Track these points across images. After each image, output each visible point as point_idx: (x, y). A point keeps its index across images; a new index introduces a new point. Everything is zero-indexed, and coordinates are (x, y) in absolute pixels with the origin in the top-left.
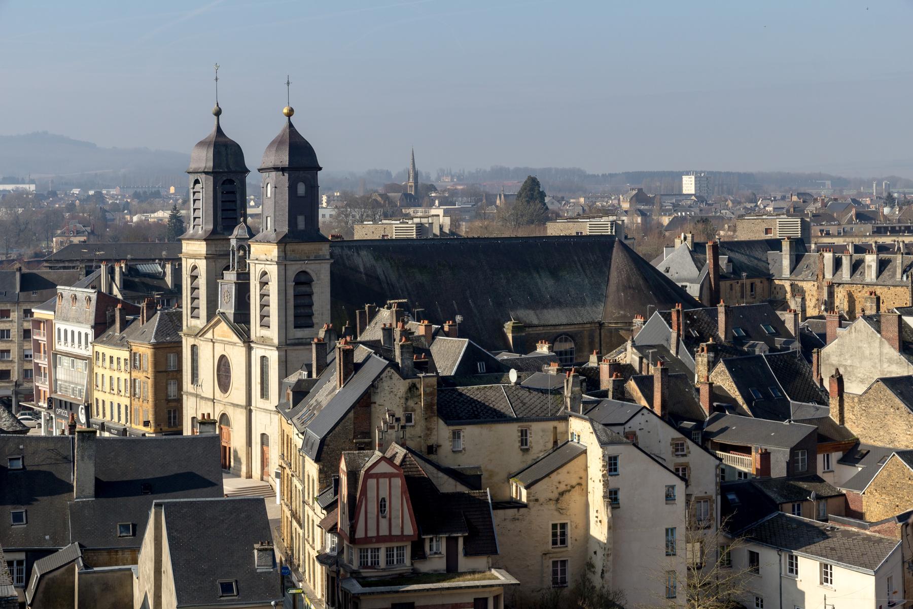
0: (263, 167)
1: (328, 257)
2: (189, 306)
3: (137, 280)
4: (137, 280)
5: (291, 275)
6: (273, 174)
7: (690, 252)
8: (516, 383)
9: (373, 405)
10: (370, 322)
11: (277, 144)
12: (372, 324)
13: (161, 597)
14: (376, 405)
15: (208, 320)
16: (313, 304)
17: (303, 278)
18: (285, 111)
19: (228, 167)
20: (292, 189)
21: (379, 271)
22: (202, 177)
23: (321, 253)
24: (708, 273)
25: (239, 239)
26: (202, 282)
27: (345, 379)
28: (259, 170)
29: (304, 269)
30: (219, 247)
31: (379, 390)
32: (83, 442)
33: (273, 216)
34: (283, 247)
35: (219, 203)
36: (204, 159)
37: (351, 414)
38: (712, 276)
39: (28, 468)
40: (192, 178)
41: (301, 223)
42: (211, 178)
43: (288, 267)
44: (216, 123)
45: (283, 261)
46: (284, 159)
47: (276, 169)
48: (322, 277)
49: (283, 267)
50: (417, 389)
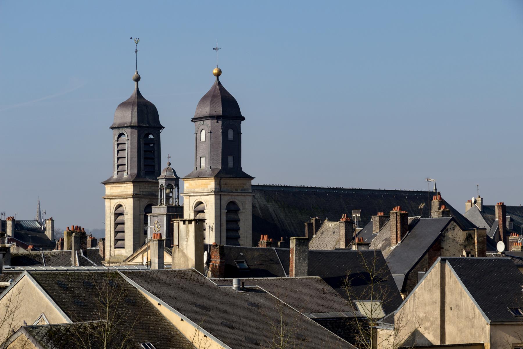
0: (198, 116)
1: (250, 191)
2: (113, 239)
3: (23, 232)
4: (23, 232)
5: (224, 204)
6: (209, 122)
7: (480, 212)
8: (503, 253)
9: (442, 250)
10: (316, 232)
11: (209, 97)
12: (319, 233)
13: (445, 329)
14: (444, 250)
15: (135, 250)
16: (239, 229)
17: (232, 207)
18: (215, 71)
19: (149, 123)
20: (225, 134)
21: (271, 210)
22: (128, 132)
23: (245, 187)
24: (498, 228)
25: (167, 179)
26: (128, 219)
27: (402, 237)
28: (193, 120)
29: (233, 200)
30: (146, 189)
31: (445, 238)
32: (299, 246)
33: (207, 156)
34: (218, 181)
35: (142, 152)
36: (129, 116)
37: (427, 256)
38: (501, 230)
39: (252, 267)
40: (117, 132)
41: (231, 164)
42: (136, 131)
43: (222, 197)
44: (136, 87)
45: (218, 192)
46: (219, 110)
47: (211, 117)
48: (246, 206)
49: (219, 197)
50: (472, 238)
